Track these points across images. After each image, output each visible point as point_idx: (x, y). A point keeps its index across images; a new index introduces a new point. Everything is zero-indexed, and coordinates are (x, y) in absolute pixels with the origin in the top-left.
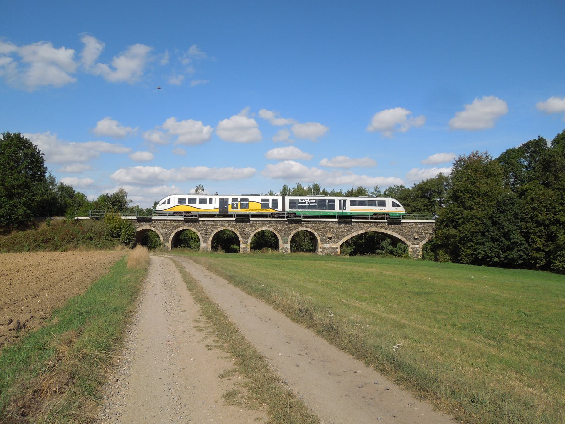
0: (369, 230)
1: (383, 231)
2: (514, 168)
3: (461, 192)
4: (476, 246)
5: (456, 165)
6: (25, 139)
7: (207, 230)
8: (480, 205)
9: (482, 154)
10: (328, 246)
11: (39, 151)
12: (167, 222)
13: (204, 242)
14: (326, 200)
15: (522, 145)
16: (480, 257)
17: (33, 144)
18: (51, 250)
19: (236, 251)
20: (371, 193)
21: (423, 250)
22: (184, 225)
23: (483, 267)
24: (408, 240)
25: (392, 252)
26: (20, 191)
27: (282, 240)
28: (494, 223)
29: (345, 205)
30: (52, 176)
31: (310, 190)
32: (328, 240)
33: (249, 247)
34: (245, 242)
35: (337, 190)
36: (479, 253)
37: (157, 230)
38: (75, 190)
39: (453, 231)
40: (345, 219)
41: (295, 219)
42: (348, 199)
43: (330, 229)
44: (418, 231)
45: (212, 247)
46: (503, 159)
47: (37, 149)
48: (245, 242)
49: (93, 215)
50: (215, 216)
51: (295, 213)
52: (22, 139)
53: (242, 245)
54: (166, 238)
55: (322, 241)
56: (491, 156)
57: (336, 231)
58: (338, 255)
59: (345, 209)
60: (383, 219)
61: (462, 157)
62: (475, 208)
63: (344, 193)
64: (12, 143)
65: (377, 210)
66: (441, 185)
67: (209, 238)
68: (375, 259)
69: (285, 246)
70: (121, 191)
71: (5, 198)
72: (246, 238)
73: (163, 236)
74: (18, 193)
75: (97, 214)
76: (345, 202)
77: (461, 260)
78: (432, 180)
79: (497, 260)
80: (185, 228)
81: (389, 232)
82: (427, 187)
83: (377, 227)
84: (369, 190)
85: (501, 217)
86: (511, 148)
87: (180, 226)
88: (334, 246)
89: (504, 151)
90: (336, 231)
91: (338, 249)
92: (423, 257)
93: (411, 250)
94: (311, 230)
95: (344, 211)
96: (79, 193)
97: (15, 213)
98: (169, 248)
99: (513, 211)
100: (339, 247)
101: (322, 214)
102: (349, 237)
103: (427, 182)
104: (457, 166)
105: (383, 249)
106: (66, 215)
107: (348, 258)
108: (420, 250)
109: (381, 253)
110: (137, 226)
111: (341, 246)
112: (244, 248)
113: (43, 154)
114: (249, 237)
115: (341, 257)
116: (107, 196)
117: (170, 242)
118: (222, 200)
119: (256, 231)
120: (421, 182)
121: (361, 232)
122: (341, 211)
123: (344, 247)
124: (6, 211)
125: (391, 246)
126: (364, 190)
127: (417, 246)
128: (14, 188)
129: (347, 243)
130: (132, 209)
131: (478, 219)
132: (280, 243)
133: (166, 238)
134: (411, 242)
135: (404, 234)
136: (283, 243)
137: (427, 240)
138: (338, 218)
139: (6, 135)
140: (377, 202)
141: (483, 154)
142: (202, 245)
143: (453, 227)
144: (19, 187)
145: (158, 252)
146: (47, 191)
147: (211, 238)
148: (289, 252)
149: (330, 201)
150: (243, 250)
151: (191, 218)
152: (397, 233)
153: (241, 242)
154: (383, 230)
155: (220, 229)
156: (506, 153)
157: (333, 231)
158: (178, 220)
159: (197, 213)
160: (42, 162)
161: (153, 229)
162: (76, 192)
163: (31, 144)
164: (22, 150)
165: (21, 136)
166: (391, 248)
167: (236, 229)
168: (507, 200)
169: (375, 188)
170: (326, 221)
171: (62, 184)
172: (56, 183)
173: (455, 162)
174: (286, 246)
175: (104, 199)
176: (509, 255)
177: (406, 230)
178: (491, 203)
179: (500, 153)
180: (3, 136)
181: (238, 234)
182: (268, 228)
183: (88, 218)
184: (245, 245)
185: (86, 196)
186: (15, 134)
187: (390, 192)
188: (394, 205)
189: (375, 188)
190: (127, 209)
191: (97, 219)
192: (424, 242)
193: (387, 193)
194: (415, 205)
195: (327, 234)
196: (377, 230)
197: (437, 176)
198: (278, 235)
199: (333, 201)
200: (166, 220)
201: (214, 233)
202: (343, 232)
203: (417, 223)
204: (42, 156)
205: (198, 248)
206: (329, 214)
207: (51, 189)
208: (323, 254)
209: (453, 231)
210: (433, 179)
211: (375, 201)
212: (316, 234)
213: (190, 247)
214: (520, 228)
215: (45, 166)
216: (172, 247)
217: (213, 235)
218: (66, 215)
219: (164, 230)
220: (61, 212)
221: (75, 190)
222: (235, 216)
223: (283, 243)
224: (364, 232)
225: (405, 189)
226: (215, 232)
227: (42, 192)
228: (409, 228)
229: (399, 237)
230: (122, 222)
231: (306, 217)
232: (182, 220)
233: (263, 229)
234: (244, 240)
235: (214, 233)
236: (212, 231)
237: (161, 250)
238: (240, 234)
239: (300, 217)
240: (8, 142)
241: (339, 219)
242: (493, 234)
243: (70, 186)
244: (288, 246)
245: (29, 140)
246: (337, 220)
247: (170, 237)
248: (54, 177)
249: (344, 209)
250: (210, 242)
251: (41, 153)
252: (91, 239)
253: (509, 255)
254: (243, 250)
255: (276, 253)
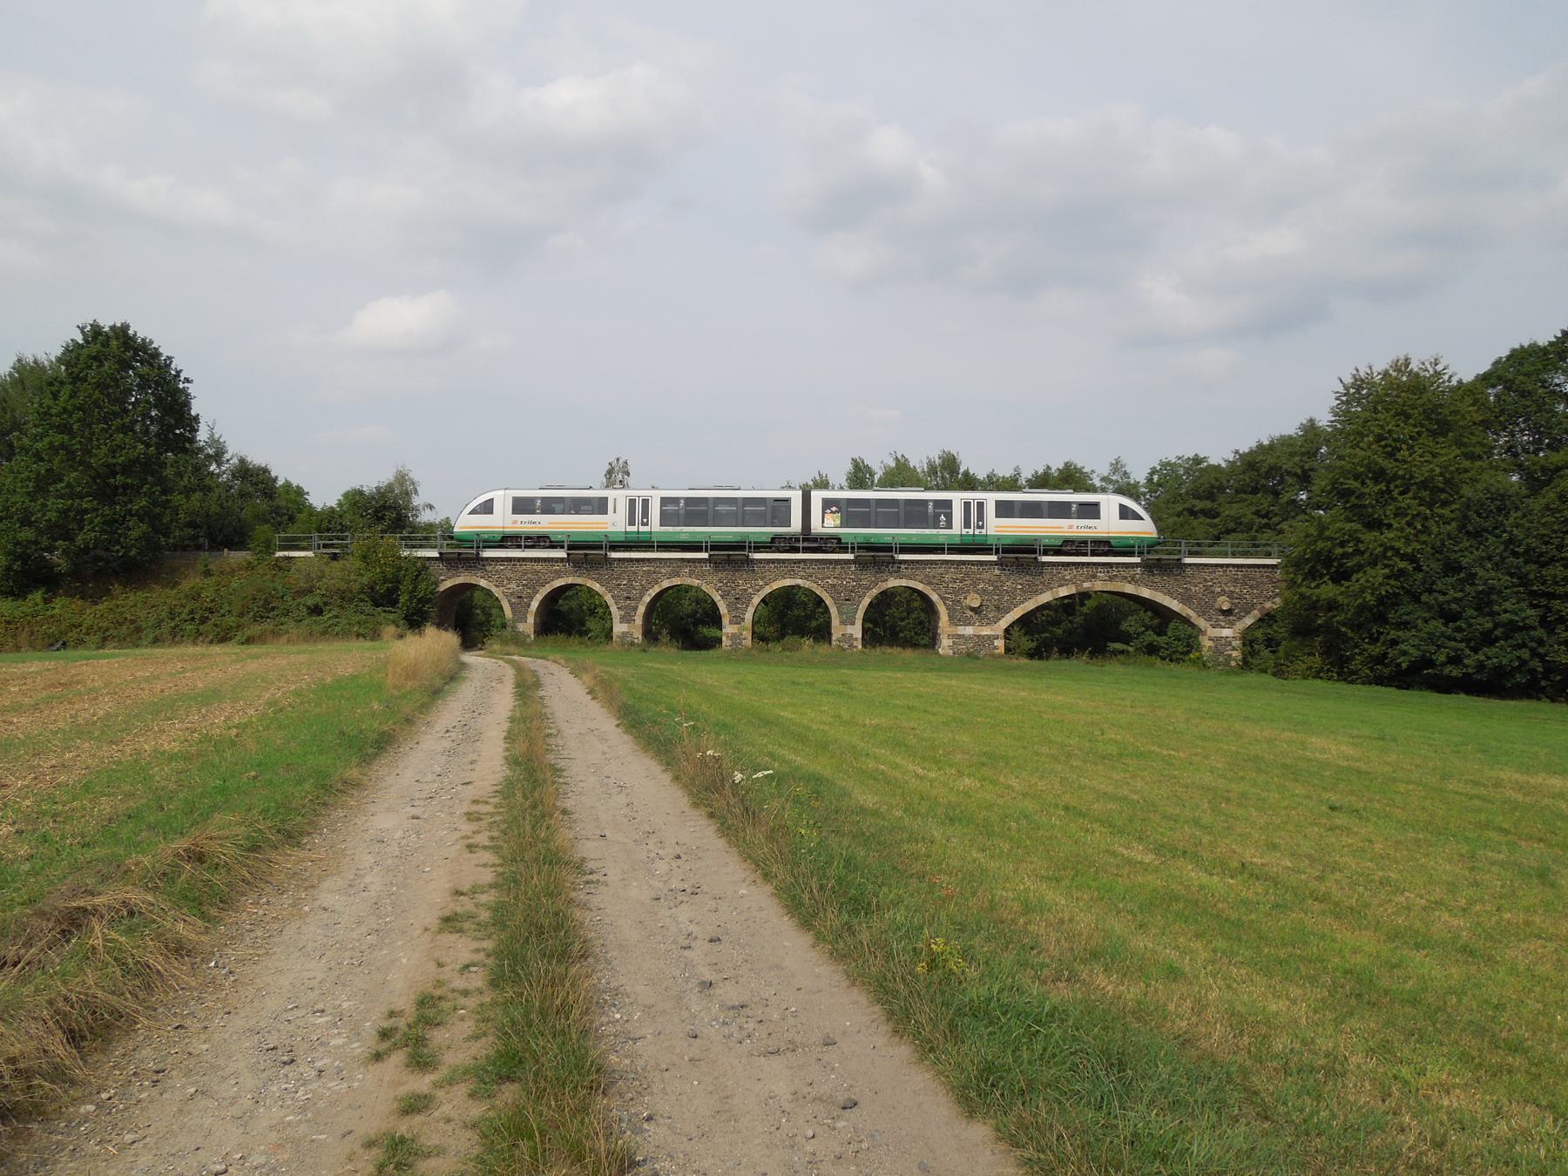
0: (1086, 585)
1: (1129, 589)
2: (1528, 403)
3: (1356, 478)
4: (1393, 634)
5: (1344, 398)
6: (139, 340)
7: (630, 586)
8: (1409, 517)
9: (1423, 364)
10: (969, 631)
11: (178, 373)
12: (521, 565)
13: (623, 619)
14: (926, 502)
15: (1560, 335)
16: (1403, 665)
17: (161, 354)
18: (211, 642)
19: (713, 643)
20: (1103, 479)
21: (1244, 645)
22: (567, 574)
23: (1414, 696)
24: (1202, 614)
25: (1152, 650)
26: (129, 481)
27: (839, 612)
28: (1452, 568)
29: (645, 514)
30: (217, 436)
31: (933, 470)
32: (969, 613)
33: (748, 634)
34: (737, 620)
35: (1005, 472)
36: (1404, 653)
37: (496, 586)
38: (277, 477)
39: (1328, 590)
40: (1020, 555)
41: (876, 556)
42: (991, 498)
43: (975, 584)
44: (1232, 589)
45: (759, 637)
46: (1500, 378)
47: (173, 366)
48: (737, 620)
49: (325, 546)
50: (653, 547)
51: (839, 540)
52: (133, 338)
53: (729, 629)
54: (520, 607)
55: (951, 617)
56: (1449, 372)
57: (991, 588)
58: (1000, 656)
59: (982, 527)
60: (1131, 554)
61: (1362, 375)
62: (1396, 525)
63: (1023, 481)
64: (106, 350)
65: (1075, 529)
66: (1313, 454)
67: (635, 609)
68: (1103, 669)
69: (848, 629)
70: (402, 478)
71: (90, 501)
72: (738, 609)
73: (511, 604)
74: (125, 487)
75: (335, 542)
76: (981, 505)
77: (1353, 673)
78: (1286, 442)
79: (1455, 672)
80: (570, 580)
81: (1146, 593)
82: (1271, 460)
83: (1111, 579)
84: (1093, 471)
85: (1470, 549)
86: (1526, 344)
87: (558, 575)
88: (986, 631)
89: (1505, 353)
90: (991, 588)
91: (997, 638)
92: (1246, 665)
93: (1210, 643)
94: (920, 587)
95: (643, 529)
96: (288, 485)
97: (118, 542)
98: (529, 636)
99: (1505, 531)
100: (1001, 633)
101: (903, 540)
102: (1030, 605)
103: (1272, 447)
104: (1347, 403)
105: (1126, 638)
106: (251, 546)
107: (1026, 664)
108: (1237, 643)
109: (1122, 652)
110: (441, 575)
111: (1007, 631)
112: (733, 637)
113: (187, 380)
114: (747, 606)
115: (1006, 662)
116: (360, 493)
117: (531, 619)
118: (670, 508)
119: (767, 590)
120: (1254, 445)
121: (1064, 592)
122: (634, 529)
123: (1015, 633)
124: (95, 536)
125: (1150, 632)
126: (1080, 471)
127: (1226, 632)
128: (114, 474)
129: (1025, 622)
130: (430, 527)
131: (1403, 557)
132: (835, 622)
133: (520, 607)
134: (1210, 619)
135: (1190, 597)
136: (843, 623)
137: (1256, 614)
138: (997, 552)
139: (89, 328)
140: (539, 503)
141: (1427, 364)
142: (619, 628)
143: (1332, 579)
144: (127, 469)
145: (497, 647)
146: (204, 482)
147: (642, 609)
148: (860, 647)
149: (938, 503)
150: (729, 643)
151: (587, 553)
152: (1170, 594)
153: (725, 621)
154: (1128, 585)
155: (666, 584)
156: (1509, 358)
157: (984, 590)
158: (552, 559)
159: (603, 539)
160: (186, 404)
161: (483, 583)
162: (280, 482)
163: (156, 354)
164: (133, 368)
165: (131, 332)
166: (1151, 637)
167: (711, 587)
168: (1487, 499)
169: (1112, 464)
170: (964, 563)
171: (242, 461)
172: (227, 456)
173: (1342, 390)
174: (850, 630)
175: (356, 500)
176: (1489, 658)
177: (1196, 586)
178: (1445, 511)
179: (1492, 360)
180: (83, 332)
181: (717, 598)
182: (800, 582)
183: (310, 554)
184: (735, 629)
185: (308, 493)
186: (114, 326)
187: (1165, 476)
188: (1125, 513)
189: (1112, 464)
190: (414, 528)
191: (334, 557)
192: (1249, 621)
193: (1156, 478)
194: (1233, 513)
195: (965, 598)
196: (1111, 587)
197: (1302, 427)
198: (828, 601)
199: (948, 504)
200: (519, 559)
201: (649, 595)
202: (1012, 593)
203: (1228, 566)
204: (186, 385)
205: (608, 634)
206: (914, 540)
207: (212, 474)
208: (954, 653)
209: (1328, 590)
210: (1290, 437)
211: (1068, 504)
212: (934, 597)
213: (582, 633)
214: (1524, 581)
215: (193, 413)
216: (535, 632)
217: (647, 599)
218: (251, 546)
219: (513, 585)
220: (236, 539)
221: (277, 477)
222: (853, 548)
223: (843, 623)
224: (1073, 591)
225: (1209, 466)
226: (653, 592)
227: (190, 482)
228: (1206, 581)
229: (1175, 605)
230: (402, 566)
231: (906, 549)
232: (562, 560)
233: (788, 582)
234: (733, 614)
235: (649, 595)
236: (644, 590)
237: (505, 642)
238: (722, 597)
239: (1034, 551)
240: (95, 348)
241: (1001, 555)
242: (1441, 598)
243: (263, 465)
244: (856, 631)
245: (151, 342)
246: (994, 558)
247: (529, 605)
248: (221, 440)
249: (643, 524)
250: (639, 620)
251: (182, 379)
252: (316, 611)
253: (1489, 658)
254: (729, 643)
255: (823, 649)
